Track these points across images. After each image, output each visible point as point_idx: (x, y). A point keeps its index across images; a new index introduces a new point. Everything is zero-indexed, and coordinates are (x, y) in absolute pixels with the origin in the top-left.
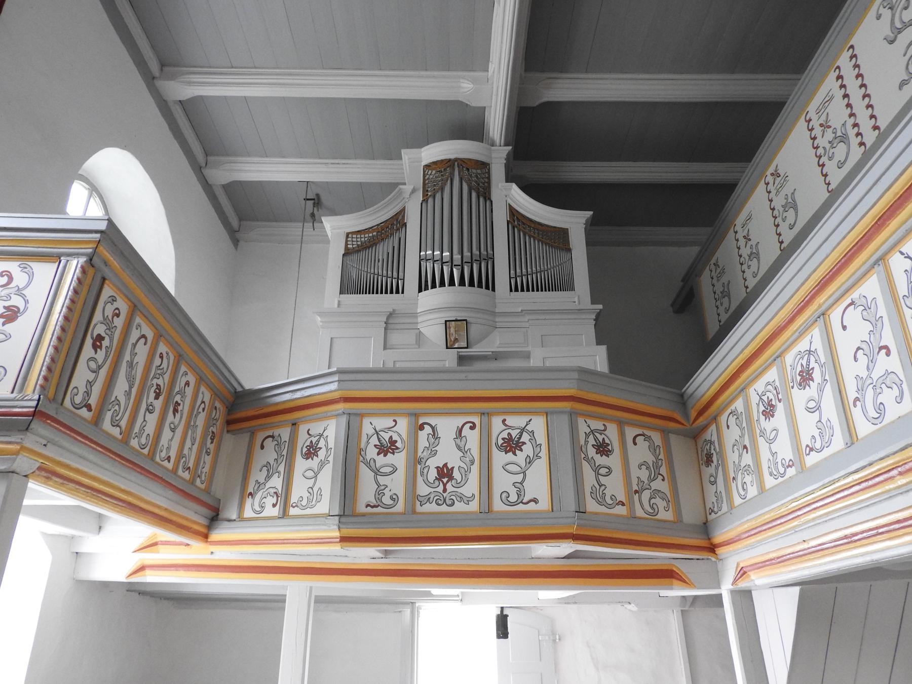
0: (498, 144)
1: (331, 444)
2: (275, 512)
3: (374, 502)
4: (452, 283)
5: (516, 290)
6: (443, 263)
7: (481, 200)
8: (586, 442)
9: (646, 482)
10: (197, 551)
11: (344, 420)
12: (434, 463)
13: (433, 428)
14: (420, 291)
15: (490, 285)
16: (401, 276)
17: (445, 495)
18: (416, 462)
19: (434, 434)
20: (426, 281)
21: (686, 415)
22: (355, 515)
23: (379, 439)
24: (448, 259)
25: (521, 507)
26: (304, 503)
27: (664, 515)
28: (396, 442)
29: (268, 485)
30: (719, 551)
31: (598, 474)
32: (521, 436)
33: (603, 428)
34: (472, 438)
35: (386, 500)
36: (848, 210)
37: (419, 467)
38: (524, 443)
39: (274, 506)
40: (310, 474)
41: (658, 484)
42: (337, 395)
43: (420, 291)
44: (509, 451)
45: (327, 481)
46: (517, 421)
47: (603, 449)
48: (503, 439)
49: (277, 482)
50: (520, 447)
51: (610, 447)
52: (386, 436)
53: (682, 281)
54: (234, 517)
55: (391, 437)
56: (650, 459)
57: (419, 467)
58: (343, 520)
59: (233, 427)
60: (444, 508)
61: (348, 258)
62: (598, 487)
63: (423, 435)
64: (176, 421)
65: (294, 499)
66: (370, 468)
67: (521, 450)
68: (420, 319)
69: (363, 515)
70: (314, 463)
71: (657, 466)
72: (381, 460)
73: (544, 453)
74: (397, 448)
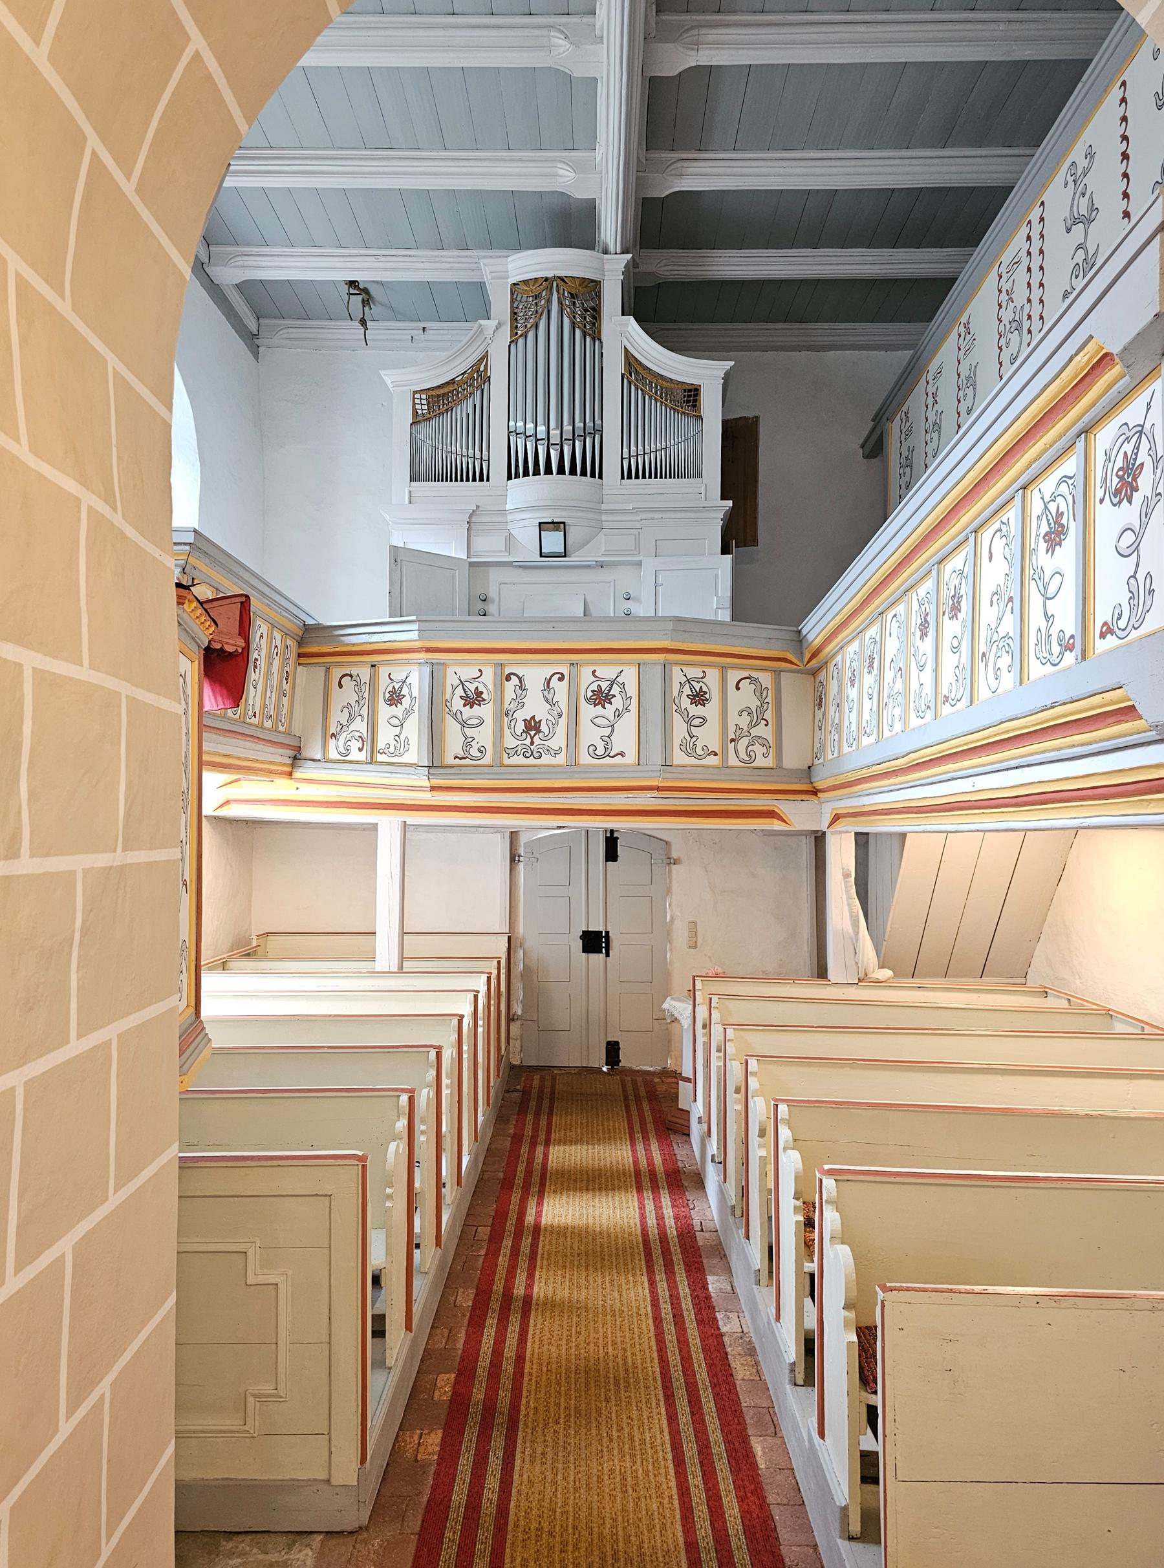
0: (613, 251)
1: (415, 693)
2: (362, 756)
3: (461, 754)
4: (548, 471)
6: (537, 440)
7: (588, 339)
8: (680, 692)
9: (746, 728)
10: (282, 788)
11: (427, 670)
12: (522, 715)
13: (520, 679)
14: (509, 478)
15: (594, 470)
18: (503, 714)
19: (522, 686)
20: (517, 466)
21: (801, 655)
24: (544, 436)
25: (607, 760)
26: (392, 750)
27: (760, 762)
29: (351, 728)
30: (820, 794)
31: (690, 724)
33: (702, 675)
34: (561, 689)
35: (474, 752)
36: (898, 528)
39: (360, 750)
40: (395, 721)
41: (760, 730)
42: (417, 645)
43: (509, 478)
45: (414, 729)
46: (607, 672)
47: (699, 698)
49: (360, 725)
51: (707, 696)
52: (471, 687)
53: (873, 420)
54: (318, 757)
56: (754, 703)
58: (432, 771)
59: (303, 660)
62: (688, 738)
63: (510, 686)
64: (257, 677)
65: (380, 745)
66: (456, 719)
68: (509, 518)
70: (398, 710)
71: (761, 711)
72: (467, 712)
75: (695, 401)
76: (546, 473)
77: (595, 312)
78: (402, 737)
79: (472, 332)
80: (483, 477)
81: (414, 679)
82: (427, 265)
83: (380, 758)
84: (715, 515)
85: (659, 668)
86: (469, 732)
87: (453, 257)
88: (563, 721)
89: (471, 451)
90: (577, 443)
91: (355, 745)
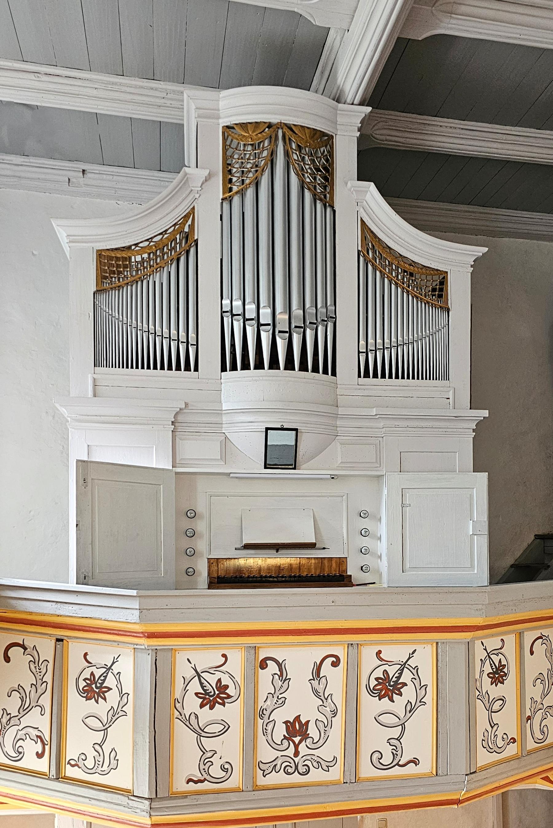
0: (349, 100)
4: (290, 365)
5: (367, 375)
8: (482, 671)
9: (539, 700)
11: (147, 661)
12: (282, 716)
13: (279, 665)
15: (324, 364)
16: (192, 341)
17: (296, 760)
18: (257, 715)
19: (282, 674)
22: (171, 797)
23: (201, 684)
24: (253, 315)
26: (90, 763)
28: (227, 687)
29: (25, 721)
32: (401, 674)
34: (335, 678)
37: (260, 722)
38: (405, 684)
40: (94, 723)
42: (137, 628)
44: (384, 696)
45: (127, 740)
46: (395, 652)
48: (377, 679)
49: (39, 721)
50: (399, 689)
51: (505, 670)
52: (212, 680)
55: (219, 680)
57: (260, 722)
58: (155, 805)
60: (296, 778)
61: (103, 297)
62: (489, 729)
66: (189, 726)
67: (401, 694)
68: (225, 419)
69: (184, 795)
70: (101, 708)
72: (206, 715)
73: (430, 698)
74: (229, 697)
75: (441, 290)
76: (270, 368)
77: (327, 172)
78: (107, 748)
79: (171, 186)
80: (189, 365)
81: (126, 666)
82: (101, 94)
83: (70, 772)
84: (466, 425)
85: (464, 648)
86: (208, 743)
87: (136, 87)
88: (338, 721)
89: (173, 332)
90: (308, 331)
91: (31, 748)
